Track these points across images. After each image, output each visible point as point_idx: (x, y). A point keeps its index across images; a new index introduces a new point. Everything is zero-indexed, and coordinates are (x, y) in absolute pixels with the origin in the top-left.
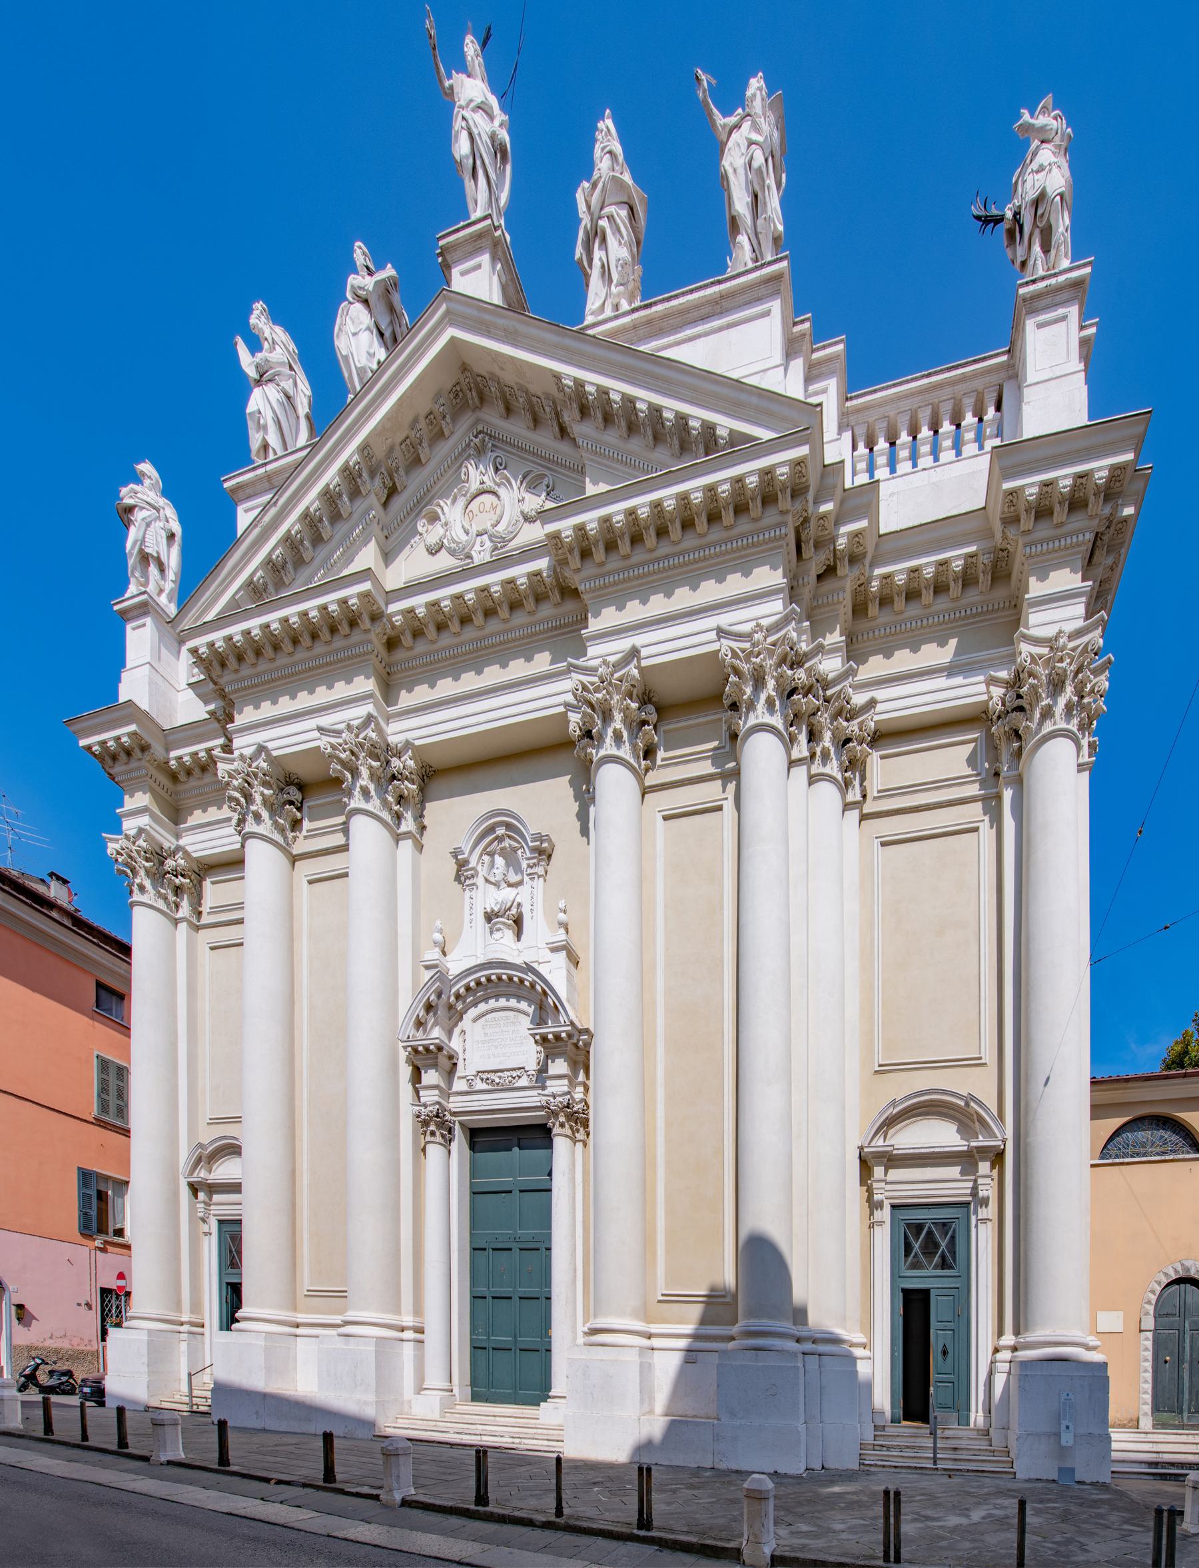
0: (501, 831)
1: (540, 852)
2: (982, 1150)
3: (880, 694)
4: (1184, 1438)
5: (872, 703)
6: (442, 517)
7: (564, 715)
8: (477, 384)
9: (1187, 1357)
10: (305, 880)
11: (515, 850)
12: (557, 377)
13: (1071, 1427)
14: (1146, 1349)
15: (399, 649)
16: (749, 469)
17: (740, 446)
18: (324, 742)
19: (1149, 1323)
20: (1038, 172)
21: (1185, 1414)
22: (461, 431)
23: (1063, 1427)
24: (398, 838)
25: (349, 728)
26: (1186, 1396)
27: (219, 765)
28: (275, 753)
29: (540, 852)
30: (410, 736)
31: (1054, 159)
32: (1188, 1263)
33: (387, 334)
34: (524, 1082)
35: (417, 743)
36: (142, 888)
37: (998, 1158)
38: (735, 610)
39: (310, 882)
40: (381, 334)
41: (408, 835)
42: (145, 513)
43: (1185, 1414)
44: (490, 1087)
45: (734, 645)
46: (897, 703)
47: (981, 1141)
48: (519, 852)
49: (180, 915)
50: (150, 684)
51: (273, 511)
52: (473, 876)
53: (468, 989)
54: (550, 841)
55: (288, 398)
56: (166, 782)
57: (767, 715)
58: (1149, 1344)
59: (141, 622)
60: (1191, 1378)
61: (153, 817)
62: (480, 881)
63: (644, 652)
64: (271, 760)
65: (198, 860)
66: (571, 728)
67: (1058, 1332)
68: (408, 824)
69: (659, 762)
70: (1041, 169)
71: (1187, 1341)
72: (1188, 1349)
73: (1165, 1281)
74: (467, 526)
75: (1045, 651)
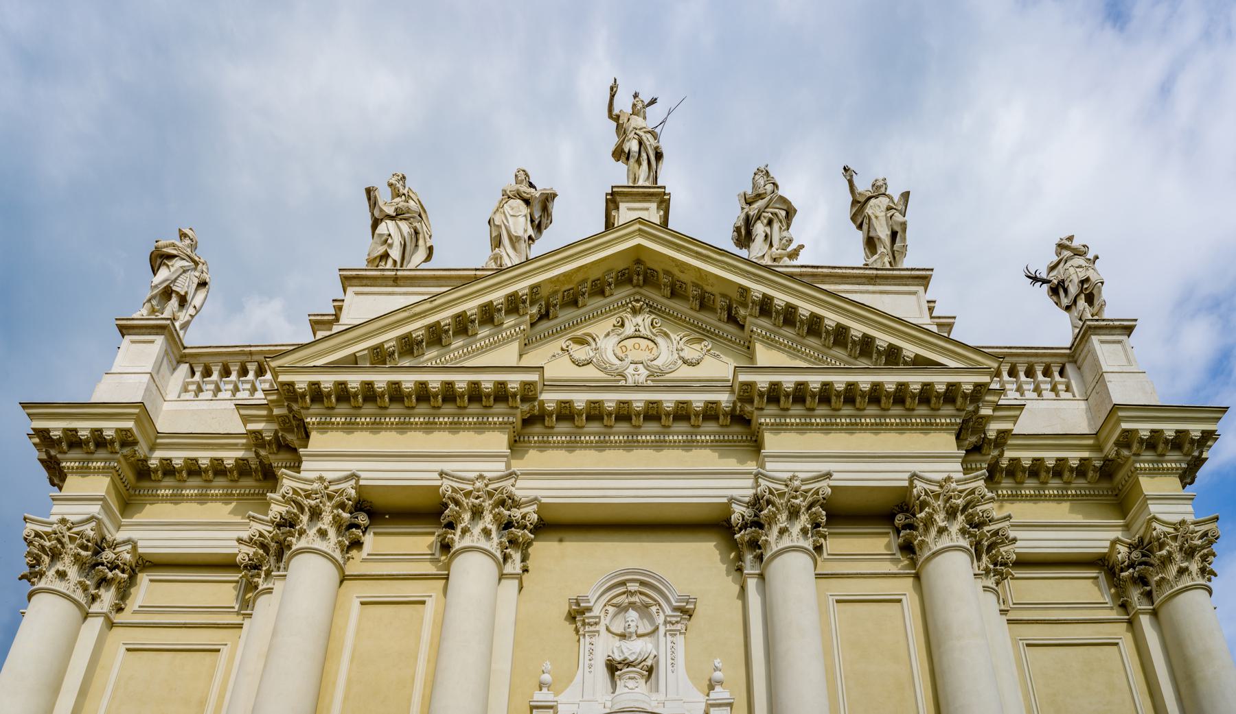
0: (633, 587)
1: (683, 611)
7: (727, 506)
11: (647, 606)
12: (745, 291)
15: (532, 418)
16: (940, 381)
17: (920, 363)
18: (446, 485)
22: (623, 293)
24: (502, 576)
25: (481, 477)
28: (362, 482)
29: (683, 611)
35: (544, 500)
36: (62, 575)
38: (922, 458)
39: (362, 603)
40: (532, 221)
41: (511, 576)
42: (184, 263)
45: (927, 487)
46: (1029, 542)
48: (654, 609)
49: (95, 608)
50: (146, 390)
51: (427, 306)
52: (596, 624)
56: (130, 475)
57: (961, 538)
61: (106, 507)
62: (601, 627)
63: (835, 476)
64: (359, 489)
65: (140, 556)
68: (514, 566)
75: (1171, 530)
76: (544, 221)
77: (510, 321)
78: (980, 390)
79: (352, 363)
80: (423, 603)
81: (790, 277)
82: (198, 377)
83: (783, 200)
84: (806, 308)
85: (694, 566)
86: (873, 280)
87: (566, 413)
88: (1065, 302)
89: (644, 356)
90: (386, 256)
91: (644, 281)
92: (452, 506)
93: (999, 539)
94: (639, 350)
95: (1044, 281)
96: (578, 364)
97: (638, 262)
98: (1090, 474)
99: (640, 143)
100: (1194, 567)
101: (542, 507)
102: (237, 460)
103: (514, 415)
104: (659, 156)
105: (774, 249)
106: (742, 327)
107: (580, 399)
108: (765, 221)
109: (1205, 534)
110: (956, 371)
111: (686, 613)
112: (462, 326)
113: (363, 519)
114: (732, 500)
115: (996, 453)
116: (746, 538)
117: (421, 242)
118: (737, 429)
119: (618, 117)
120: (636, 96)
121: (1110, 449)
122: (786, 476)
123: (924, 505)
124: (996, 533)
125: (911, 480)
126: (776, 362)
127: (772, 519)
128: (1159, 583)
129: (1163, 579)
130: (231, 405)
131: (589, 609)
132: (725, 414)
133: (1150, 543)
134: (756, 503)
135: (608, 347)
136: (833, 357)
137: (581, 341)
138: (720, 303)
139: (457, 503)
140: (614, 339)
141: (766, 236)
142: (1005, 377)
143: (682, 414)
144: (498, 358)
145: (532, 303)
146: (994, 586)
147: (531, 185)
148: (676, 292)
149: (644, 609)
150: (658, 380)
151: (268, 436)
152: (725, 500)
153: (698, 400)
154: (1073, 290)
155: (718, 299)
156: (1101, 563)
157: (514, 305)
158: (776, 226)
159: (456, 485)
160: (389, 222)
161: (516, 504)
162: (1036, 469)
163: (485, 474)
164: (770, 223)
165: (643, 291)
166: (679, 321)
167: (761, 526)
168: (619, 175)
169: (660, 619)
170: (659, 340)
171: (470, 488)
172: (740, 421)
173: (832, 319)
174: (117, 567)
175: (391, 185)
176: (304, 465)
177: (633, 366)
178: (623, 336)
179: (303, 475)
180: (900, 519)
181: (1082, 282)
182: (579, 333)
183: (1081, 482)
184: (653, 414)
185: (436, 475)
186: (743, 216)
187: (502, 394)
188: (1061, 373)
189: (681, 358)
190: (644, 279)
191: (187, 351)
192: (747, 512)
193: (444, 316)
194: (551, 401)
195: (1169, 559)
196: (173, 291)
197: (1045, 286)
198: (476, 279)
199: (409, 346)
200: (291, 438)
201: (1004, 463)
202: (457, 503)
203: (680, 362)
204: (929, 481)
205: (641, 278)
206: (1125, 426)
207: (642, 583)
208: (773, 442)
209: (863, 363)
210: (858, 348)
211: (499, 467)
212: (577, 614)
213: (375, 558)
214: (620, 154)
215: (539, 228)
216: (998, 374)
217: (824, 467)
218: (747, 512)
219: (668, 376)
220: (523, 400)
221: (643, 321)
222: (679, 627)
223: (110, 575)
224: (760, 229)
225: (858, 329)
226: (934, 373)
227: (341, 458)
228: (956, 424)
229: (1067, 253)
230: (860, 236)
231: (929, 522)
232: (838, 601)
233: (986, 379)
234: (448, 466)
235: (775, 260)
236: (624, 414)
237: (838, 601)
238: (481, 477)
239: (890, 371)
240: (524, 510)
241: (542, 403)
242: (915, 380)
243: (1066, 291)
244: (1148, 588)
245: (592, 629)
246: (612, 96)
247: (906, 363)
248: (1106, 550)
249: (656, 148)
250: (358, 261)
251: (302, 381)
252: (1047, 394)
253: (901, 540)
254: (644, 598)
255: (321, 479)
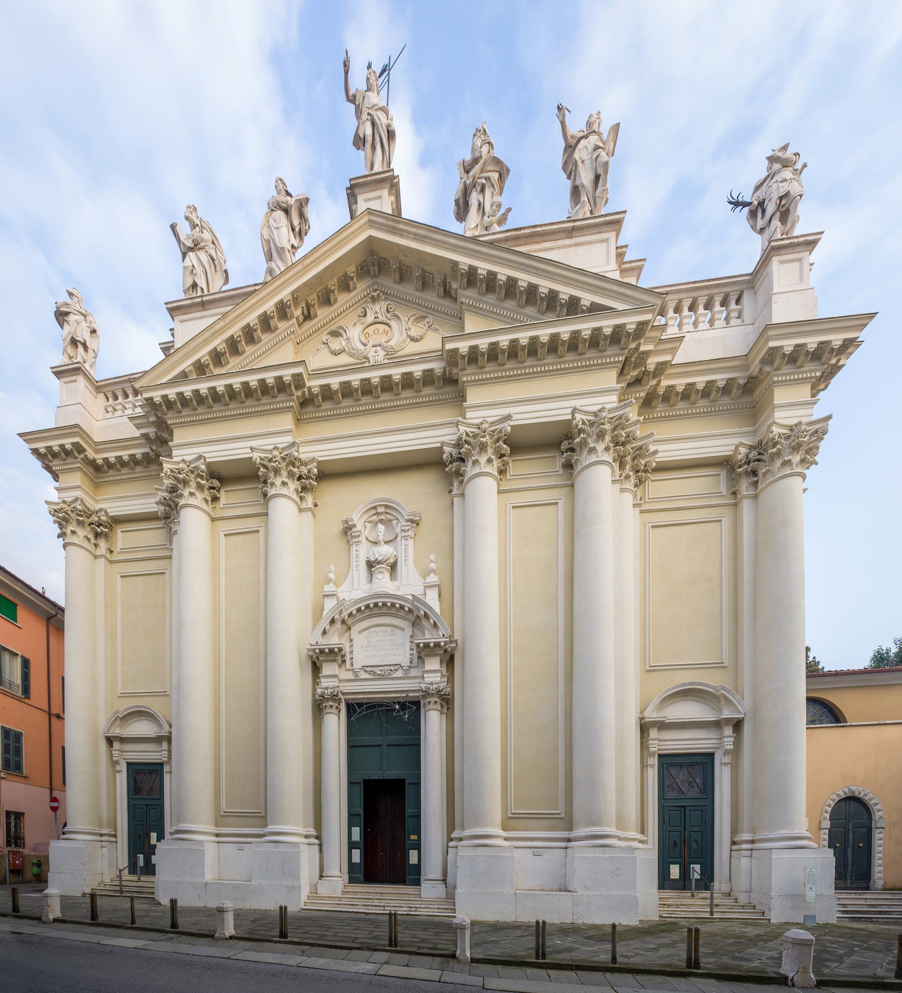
0: (381, 510)
1: (412, 521)
2: (728, 721)
3: (660, 447)
4: (853, 896)
5: (656, 452)
6: (344, 334)
7: (441, 448)
8: (379, 263)
9: (851, 843)
10: (222, 534)
11: (391, 521)
12: (455, 264)
13: (814, 888)
14: (825, 840)
15: (310, 402)
16: (607, 324)
17: (596, 309)
19: (827, 824)
20: (781, 182)
21: (849, 881)
23: (808, 888)
25: (276, 448)
26: (850, 867)
27: (164, 465)
28: (208, 460)
29: (412, 521)
30: (316, 455)
31: (793, 177)
32: (853, 788)
33: (297, 229)
34: (399, 674)
35: (320, 459)
37: (738, 725)
38: (589, 394)
39: (225, 535)
40: (293, 230)
41: (309, 510)
43: (849, 881)
44: (372, 677)
46: (666, 453)
47: (727, 714)
48: (394, 522)
51: (222, 324)
53: (393, 605)
54: (420, 516)
55: (213, 260)
58: (826, 837)
59: (73, 378)
60: (853, 857)
63: (515, 417)
66: (444, 456)
67: (796, 831)
69: (508, 477)
70: (785, 180)
71: (851, 835)
72: (851, 839)
73: (837, 799)
74: (365, 341)
76: (303, 228)
77: (282, 325)
78: (642, 327)
79: (183, 377)
80: (258, 531)
81: (491, 244)
82: (120, 399)
83: (497, 161)
84: (503, 273)
85: (412, 493)
86: (570, 232)
87: (327, 393)
88: (760, 223)
89: (382, 339)
90: (194, 286)
91: (379, 271)
92: (262, 469)
93: (640, 452)
94: (378, 335)
95: (745, 204)
96: (335, 353)
97: (372, 253)
98: (734, 391)
99: (373, 124)
100: (796, 459)
101: (319, 463)
102: (143, 454)
103: (292, 400)
104: (391, 135)
105: (486, 217)
106: (456, 299)
107: (334, 382)
108: (479, 189)
109: (816, 432)
110: (624, 313)
111: (416, 523)
112: (249, 335)
113: (216, 483)
114: (443, 443)
115: (653, 383)
116: (454, 470)
117: (218, 268)
118: (448, 389)
119: (354, 96)
120: (369, 67)
121: (754, 369)
122: (478, 421)
123: (581, 431)
124: (640, 448)
125: (573, 413)
126: (480, 329)
127: (469, 453)
128: (765, 474)
129: (769, 470)
130: (126, 419)
131: (354, 526)
132: (439, 378)
133: (767, 443)
134: (458, 444)
135: (354, 333)
136: (526, 315)
137: (335, 334)
138: (438, 280)
139: (265, 467)
140: (359, 328)
141: (479, 205)
142: (671, 314)
143: (408, 381)
144: (277, 356)
145: (296, 305)
146: (496, 473)
147: (288, 194)
148: (403, 275)
149: (387, 523)
150: (394, 358)
151: (152, 435)
152: (439, 445)
153: (417, 370)
154: (770, 208)
155: (436, 276)
156: (725, 463)
157: (283, 310)
158: (488, 192)
159: (262, 455)
160: (190, 254)
161: (303, 463)
162: (688, 394)
163: (278, 446)
164: (483, 190)
165: (379, 280)
166: (406, 302)
167: (463, 460)
168: (357, 164)
169: (398, 530)
170: (393, 323)
171: (270, 456)
172: (447, 383)
173: (524, 279)
174: (101, 525)
175: (187, 218)
176: (174, 453)
177: (374, 349)
178: (366, 325)
179: (175, 459)
180: (565, 445)
181: (781, 198)
182: (334, 328)
183: (726, 400)
184: (387, 385)
185: (249, 450)
186: (461, 186)
187: (281, 386)
188: (738, 302)
189: (409, 336)
190: (384, 268)
191: (99, 384)
192: (455, 452)
193: (235, 330)
194: (315, 386)
195: (779, 454)
196: (77, 341)
197: (746, 209)
198: (250, 294)
199: (217, 357)
200: (165, 435)
201: (661, 391)
202: (265, 467)
203: (409, 340)
204: (588, 412)
205: (376, 268)
206: (772, 344)
207: (386, 507)
208: (474, 396)
209: (550, 317)
210: (545, 304)
211: (289, 439)
212: (348, 530)
213: (227, 507)
214: (359, 142)
215: (301, 235)
216: (662, 313)
217: (505, 411)
218: (455, 452)
219: (399, 354)
220: (297, 389)
221: (378, 309)
222: (410, 533)
223: (99, 530)
224: (474, 198)
225: (545, 285)
226: (604, 318)
227: (199, 444)
228: (619, 362)
229: (777, 166)
230: (568, 184)
231: (584, 443)
232: (513, 507)
233: (648, 317)
234: (255, 443)
235: (486, 229)
236: (367, 388)
237: (513, 507)
238: (276, 448)
239: (566, 322)
240: (309, 467)
241: (310, 389)
242: (586, 327)
243: (764, 211)
244: (755, 479)
245: (356, 540)
246: (347, 73)
247: (583, 312)
248: (731, 453)
249: (388, 126)
250: (177, 294)
251: (157, 396)
252: (720, 323)
253: (563, 460)
254: (388, 516)
255: (183, 461)
